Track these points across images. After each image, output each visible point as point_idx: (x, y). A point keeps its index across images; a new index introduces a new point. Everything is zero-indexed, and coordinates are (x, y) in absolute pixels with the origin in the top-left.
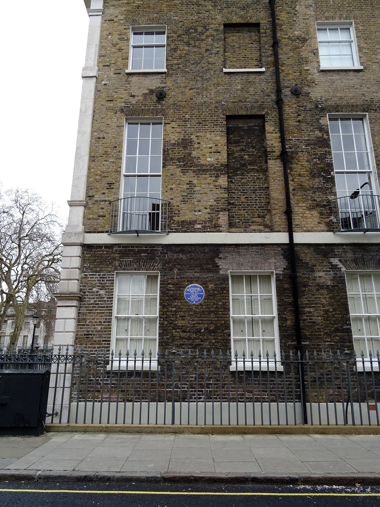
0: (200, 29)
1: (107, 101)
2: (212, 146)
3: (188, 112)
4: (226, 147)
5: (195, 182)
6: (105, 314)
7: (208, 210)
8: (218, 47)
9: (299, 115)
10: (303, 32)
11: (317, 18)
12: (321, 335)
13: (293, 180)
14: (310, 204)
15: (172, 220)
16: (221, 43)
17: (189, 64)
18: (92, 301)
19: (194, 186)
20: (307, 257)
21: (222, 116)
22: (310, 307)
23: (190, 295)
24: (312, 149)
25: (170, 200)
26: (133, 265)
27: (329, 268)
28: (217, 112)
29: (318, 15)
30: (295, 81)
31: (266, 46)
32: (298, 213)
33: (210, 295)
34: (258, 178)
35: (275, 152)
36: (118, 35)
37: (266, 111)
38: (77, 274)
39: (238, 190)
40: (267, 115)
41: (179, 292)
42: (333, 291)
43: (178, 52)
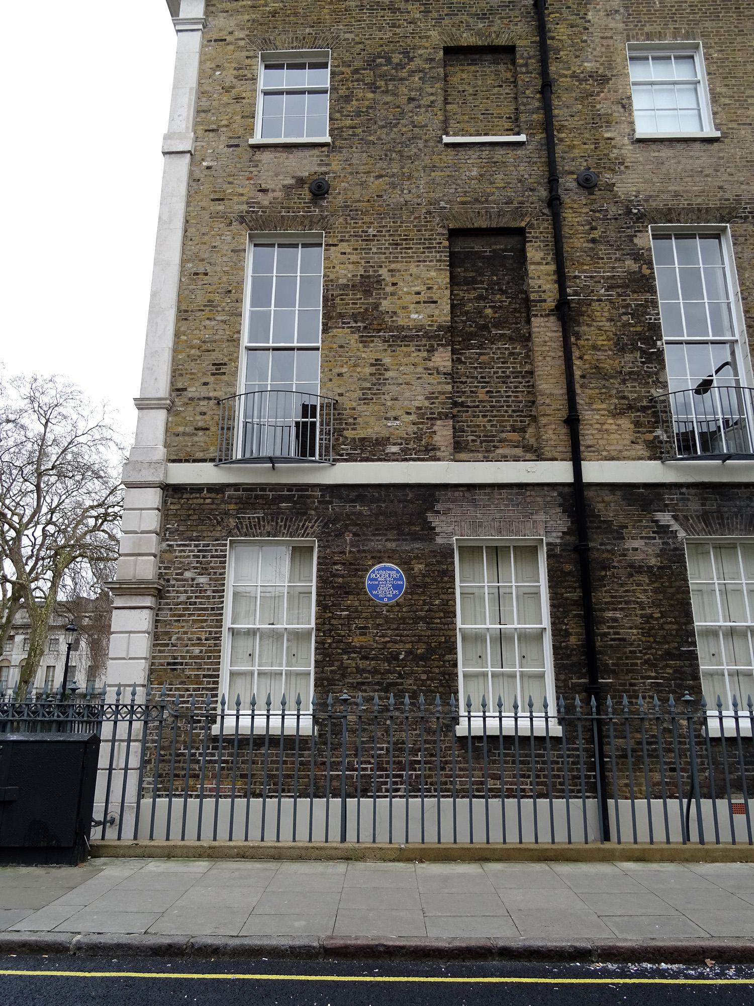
0: (396, 58)
1: (213, 200)
2: (420, 289)
3: (372, 223)
4: (448, 292)
5: (387, 360)
6: (209, 623)
7: (413, 417)
8: (432, 94)
9: (594, 228)
10: (601, 64)
11: (628, 36)
12: (636, 664)
13: (581, 358)
14: (616, 405)
15: (342, 436)
16: (438, 85)
17: (376, 127)
18: (183, 597)
19: (386, 370)
20: (609, 510)
21: (440, 230)
22: (615, 610)
23: (378, 585)
24: (619, 295)
25: (337, 398)
26: (264, 526)
27: (654, 532)
28: (430, 222)
29: (630, 30)
30: (586, 160)
31: (527, 92)
32: (591, 422)
33: (416, 586)
34: (511, 354)
35: (545, 301)
36: (235, 69)
37: (528, 220)
38: (152, 543)
39: (473, 377)
40: (530, 228)
41: (354, 580)
42: (662, 578)
43: (354, 103)
